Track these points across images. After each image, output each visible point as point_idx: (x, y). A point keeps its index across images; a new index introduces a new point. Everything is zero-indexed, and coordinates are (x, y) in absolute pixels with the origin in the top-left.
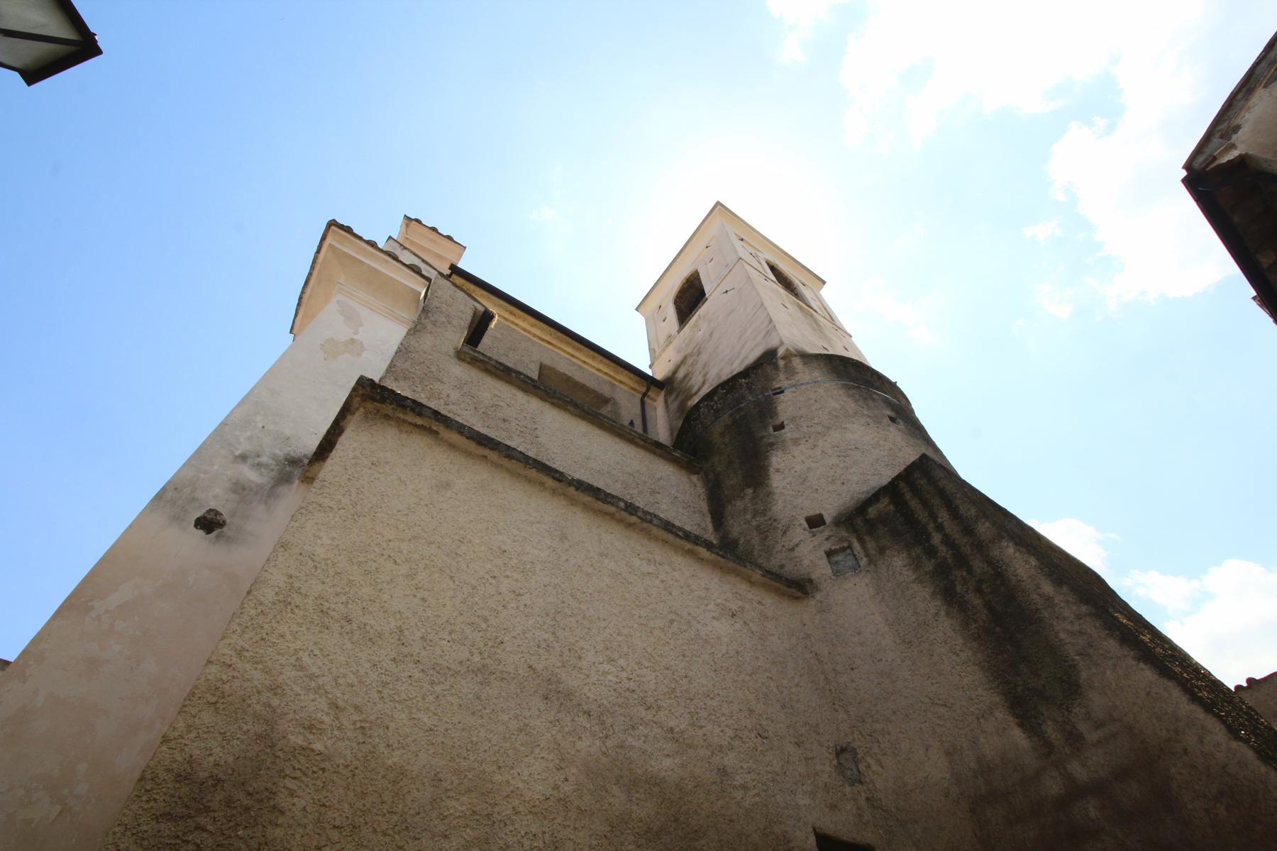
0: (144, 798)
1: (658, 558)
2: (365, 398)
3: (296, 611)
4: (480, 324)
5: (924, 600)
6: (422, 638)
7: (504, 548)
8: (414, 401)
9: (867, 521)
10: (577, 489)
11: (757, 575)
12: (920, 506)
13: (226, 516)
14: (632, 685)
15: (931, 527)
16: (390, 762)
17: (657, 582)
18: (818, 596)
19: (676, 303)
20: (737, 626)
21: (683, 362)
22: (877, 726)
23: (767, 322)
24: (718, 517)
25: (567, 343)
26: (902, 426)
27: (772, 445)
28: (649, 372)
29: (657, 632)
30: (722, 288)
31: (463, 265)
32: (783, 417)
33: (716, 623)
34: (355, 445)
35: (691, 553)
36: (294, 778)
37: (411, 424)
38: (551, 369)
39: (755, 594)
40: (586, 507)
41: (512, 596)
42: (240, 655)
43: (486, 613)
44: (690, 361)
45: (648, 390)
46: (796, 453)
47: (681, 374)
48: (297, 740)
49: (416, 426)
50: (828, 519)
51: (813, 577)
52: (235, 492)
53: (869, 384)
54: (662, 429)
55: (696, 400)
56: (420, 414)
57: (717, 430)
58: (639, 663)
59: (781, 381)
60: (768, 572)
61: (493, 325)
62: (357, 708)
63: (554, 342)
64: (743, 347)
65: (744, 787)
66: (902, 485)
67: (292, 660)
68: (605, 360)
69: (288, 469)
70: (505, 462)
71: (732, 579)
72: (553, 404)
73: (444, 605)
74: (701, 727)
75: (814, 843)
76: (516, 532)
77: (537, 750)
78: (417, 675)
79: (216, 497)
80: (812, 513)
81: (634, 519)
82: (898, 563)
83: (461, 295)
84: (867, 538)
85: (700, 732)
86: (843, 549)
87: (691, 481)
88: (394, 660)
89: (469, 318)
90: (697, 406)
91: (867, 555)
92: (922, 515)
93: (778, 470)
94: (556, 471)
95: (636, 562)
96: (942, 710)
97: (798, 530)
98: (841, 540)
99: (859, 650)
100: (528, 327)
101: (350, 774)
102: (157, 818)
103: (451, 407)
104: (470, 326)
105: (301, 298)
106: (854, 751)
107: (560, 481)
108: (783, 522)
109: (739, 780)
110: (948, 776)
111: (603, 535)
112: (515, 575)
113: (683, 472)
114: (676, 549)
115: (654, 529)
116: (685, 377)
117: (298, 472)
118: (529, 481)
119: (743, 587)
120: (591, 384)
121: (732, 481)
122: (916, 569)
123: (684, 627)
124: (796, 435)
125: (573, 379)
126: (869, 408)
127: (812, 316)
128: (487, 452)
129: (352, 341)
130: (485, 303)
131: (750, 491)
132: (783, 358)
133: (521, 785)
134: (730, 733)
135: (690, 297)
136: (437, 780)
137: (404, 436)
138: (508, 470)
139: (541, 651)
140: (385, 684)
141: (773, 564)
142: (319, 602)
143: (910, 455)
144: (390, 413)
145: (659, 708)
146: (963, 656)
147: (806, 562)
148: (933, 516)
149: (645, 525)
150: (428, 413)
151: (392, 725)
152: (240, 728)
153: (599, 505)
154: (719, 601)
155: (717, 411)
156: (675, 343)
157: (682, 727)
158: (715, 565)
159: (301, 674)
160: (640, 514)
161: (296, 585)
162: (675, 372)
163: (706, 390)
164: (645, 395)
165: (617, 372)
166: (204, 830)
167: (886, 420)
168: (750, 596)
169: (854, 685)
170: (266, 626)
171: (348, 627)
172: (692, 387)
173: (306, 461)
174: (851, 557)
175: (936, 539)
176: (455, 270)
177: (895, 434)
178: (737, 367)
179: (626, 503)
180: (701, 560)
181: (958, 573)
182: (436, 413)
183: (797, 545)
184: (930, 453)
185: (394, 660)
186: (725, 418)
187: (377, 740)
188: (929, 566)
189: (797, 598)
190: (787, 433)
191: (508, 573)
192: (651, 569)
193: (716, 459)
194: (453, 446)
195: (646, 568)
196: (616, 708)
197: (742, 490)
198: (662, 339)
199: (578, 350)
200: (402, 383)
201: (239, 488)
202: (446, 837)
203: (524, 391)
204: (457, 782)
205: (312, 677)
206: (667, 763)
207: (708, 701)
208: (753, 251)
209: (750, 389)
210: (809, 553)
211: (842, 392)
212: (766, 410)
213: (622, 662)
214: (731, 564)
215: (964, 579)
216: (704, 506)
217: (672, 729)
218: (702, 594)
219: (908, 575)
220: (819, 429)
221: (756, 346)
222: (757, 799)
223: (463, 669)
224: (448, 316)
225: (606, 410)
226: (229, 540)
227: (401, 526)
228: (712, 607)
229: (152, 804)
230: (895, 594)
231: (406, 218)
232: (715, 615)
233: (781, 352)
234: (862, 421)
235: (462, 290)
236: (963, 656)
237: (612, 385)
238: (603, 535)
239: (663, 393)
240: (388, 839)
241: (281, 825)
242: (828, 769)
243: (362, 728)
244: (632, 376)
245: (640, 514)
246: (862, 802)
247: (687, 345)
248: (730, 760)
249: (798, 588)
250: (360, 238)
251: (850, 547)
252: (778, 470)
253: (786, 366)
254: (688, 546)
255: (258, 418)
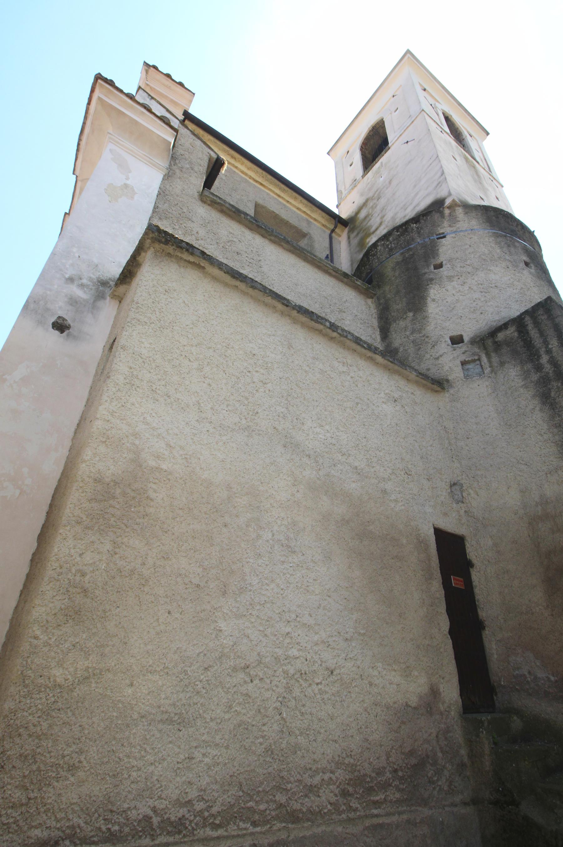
0: (80, 491)
1: (349, 362)
2: (154, 240)
3: (138, 389)
4: (215, 166)
5: (527, 400)
6: (212, 408)
7: (254, 352)
8: (187, 244)
9: (495, 343)
10: (298, 312)
11: (413, 375)
12: (538, 335)
13: (70, 322)
14: (334, 441)
15: (542, 351)
16: (203, 477)
17: (349, 378)
18: (452, 391)
19: (362, 149)
20: (398, 408)
21: (365, 204)
22: (479, 473)
23: (439, 174)
24: (385, 332)
25: (276, 185)
26: (533, 271)
27: (432, 280)
28: (336, 211)
29: (348, 410)
30: (404, 139)
31: (192, 111)
32: (442, 258)
33: (384, 406)
34: (153, 276)
35: (371, 359)
36: (155, 483)
37: (185, 260)
38: (263, 207)
39: (410, 388)
40: (303, 325)
41: (261, 384)
42: (112, 415)
43: (246, 394)
44: (371, 204)
45: (336, 227)
46: (449, 288)
47: (362, 215)
48: (152, 463)
49: (189, 262)
50: (466, 339)
51: (450, 378)
52: (71, 305)
53: (513, 233)
54: (345, 260)
55: (373, 239)
56: (192, 254)
57: (390, 267)
58: (337, 428)
59: (445, 227)
60: (420, 373)
61: (223, 171)
62: (182, 448)
63: (264, 183)
64: (417, 194)
65: (396, 501)
66: (528, 319)
67: (142, 419)
68: (305, 202)
69: (101, 288)
70: (250, 291)
71: (396, 377)
72: (270, 240)
73: (222, 389)
74: (373, 467)
75: (433, 532)
76: (260, 342)
77: (281, 475)
78: (212, 430)
79: (60, 308)
80: (455, 333)
81: (335, 334)
82: (513, 373)
83: (198, 143)
84: (493, 355)
85: (372, 470)
86: (474, 361)
87: (367, 304)
88: (197, 421)
89: (206, 165)
90: (375, 245)
91: (491, 366)
92: (537, 342)
93: (434, 300)
94: (285, 299)
95: (336, 364)
96: (523, 467)
97: (443, 345)
98: (474, 354)
99: (475, 427)
100: (245, 170)
101: (183, 482)
102: (90, 501)
103: (200, 242)
104: (207, 172)
105: (79, 144)
106: (462, 485)
107: (287, 306)
108: (433, 339)
109: (393, 497)
110: (519, 504)
111: (315, 345)
112: (262, 371)
113: (362, 296)
114: (361, 356)
115: (348, 341)
116: (366, 218)
117: (108, 292)
118: (266, 305)
119: (402, 383)
120: (293, 221)
121: (398, 306)
122: (525, 379)
123: (365, 408)
124: (451, 273)
125: (279, 216)
126: (511, 254)
127: (474, 167)
128: (238, 283)
129: (126, 186)
130: (216, 150)
131: (411, 314)
132: (449, 208)
133: (274, 493)
134: (390, 471)
135: (375, 145)
136: (229, 487)
137: (182, 270)
138: (251, 297)
139: (280, 419)
140: (195, 435)
141: (423, 368)
142: (150, 384)
143: (537, 296)
144: (171, 252)
145: (349, 455)
146: (546, 437)
147: (446, 368)
148: (546, 343)
149: (342, 339)
150: (198, 253)
151: (202, 458)
152: (121, 456)
153: (313, 324)
154: (387, 391)
155: (391, 250)
156: (360, 186)
157: (362, 466)
158: (385, 367)
159: (147, 427)
160: (339, 331)
161: (135, 373)
162: (357, 213)
163: (383, 231)
164: (333, 231)
165: (313, 211)
166: (114, 507)
167: (522, 265)
168: (407, 389)
169: (467, 448)
170: (123, 398)
171: (169, 400)
172: (371, 226)
173: (113, 284)
174: (479, 366)
175: (545, 359)
176: (188, 117)
177: (528, 276)
178: (410, 213)
179: (330, 323)
180: (377, 364)
181: (555, 384)
182: (203, 253)
183: (441, 356)
184: (554, 297)
185: (197, 421)
186: (397, 256)
187: (195, 465)
188: (535, 377)
189: (436, 391)
190: (444, 271)
191: (257, 369)
192: (345, 369)
193: (387, 288)
194: (215, 279)
195: (342, 368)
196: (325, 454)
197: (406, 313)
198: (348, 182)
199: (283, 191)
200: (165, 222)
201: (73, 302)
202: (237, 516)
203: (251, 229)
204: (240, 489)
205: (154, 429)
206: (353, 485)
207: (377, 452)
208: (432, 102)
209: (419, 233)
210: (449, 362)
211: (491, 239)
212: (430, 251)
213: (327, 427)
214: (396, 367)
215: (558, 388)
216: (375, 323)
217: (356, 468)
218: (377, 387)
219: (519, 382)
220: (469, 269)
221: (427, 195)
222: (403, 507)
223: (237, 428)
224: (190, 163)
225: (303, 243)
226: (75, 338)
227: (190, 336)
228: (382, 395)
229: (85, 494)
230: (506, 393)
231: (146, 64)
232: (384, 400)
233: (448, 202)
234: (504, 264)
235: (199, 138)
236: (546, 437)
237: (309, 223)
238: (315, 345)
239: (347, 230)
240: (207, 516)
241: (153, 506)
242: (444, 494)
243: (186, 458)
244: (324, 214)
245: (339, 331)
246: (462, 512)
247: (370, 189)
248: (389, 486)
249: (438, 384)
250: (121, 91)
251: (479, 360)
252: (434, 300)
253: (450, 214)
254: (369, 354)
255: (75, 250)
